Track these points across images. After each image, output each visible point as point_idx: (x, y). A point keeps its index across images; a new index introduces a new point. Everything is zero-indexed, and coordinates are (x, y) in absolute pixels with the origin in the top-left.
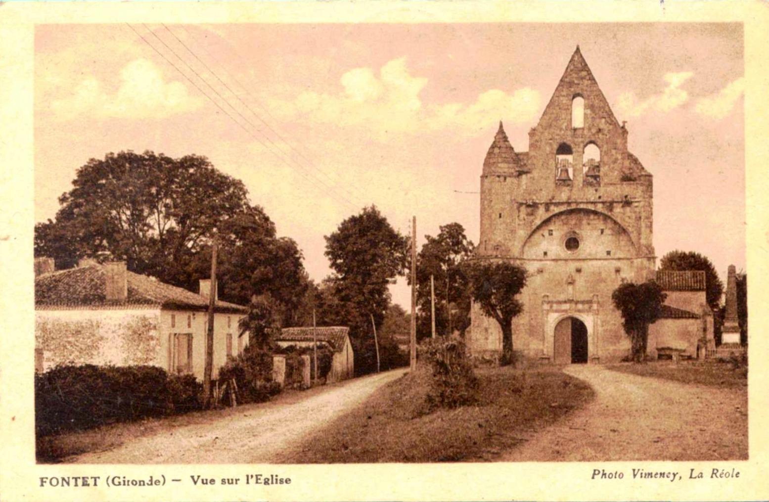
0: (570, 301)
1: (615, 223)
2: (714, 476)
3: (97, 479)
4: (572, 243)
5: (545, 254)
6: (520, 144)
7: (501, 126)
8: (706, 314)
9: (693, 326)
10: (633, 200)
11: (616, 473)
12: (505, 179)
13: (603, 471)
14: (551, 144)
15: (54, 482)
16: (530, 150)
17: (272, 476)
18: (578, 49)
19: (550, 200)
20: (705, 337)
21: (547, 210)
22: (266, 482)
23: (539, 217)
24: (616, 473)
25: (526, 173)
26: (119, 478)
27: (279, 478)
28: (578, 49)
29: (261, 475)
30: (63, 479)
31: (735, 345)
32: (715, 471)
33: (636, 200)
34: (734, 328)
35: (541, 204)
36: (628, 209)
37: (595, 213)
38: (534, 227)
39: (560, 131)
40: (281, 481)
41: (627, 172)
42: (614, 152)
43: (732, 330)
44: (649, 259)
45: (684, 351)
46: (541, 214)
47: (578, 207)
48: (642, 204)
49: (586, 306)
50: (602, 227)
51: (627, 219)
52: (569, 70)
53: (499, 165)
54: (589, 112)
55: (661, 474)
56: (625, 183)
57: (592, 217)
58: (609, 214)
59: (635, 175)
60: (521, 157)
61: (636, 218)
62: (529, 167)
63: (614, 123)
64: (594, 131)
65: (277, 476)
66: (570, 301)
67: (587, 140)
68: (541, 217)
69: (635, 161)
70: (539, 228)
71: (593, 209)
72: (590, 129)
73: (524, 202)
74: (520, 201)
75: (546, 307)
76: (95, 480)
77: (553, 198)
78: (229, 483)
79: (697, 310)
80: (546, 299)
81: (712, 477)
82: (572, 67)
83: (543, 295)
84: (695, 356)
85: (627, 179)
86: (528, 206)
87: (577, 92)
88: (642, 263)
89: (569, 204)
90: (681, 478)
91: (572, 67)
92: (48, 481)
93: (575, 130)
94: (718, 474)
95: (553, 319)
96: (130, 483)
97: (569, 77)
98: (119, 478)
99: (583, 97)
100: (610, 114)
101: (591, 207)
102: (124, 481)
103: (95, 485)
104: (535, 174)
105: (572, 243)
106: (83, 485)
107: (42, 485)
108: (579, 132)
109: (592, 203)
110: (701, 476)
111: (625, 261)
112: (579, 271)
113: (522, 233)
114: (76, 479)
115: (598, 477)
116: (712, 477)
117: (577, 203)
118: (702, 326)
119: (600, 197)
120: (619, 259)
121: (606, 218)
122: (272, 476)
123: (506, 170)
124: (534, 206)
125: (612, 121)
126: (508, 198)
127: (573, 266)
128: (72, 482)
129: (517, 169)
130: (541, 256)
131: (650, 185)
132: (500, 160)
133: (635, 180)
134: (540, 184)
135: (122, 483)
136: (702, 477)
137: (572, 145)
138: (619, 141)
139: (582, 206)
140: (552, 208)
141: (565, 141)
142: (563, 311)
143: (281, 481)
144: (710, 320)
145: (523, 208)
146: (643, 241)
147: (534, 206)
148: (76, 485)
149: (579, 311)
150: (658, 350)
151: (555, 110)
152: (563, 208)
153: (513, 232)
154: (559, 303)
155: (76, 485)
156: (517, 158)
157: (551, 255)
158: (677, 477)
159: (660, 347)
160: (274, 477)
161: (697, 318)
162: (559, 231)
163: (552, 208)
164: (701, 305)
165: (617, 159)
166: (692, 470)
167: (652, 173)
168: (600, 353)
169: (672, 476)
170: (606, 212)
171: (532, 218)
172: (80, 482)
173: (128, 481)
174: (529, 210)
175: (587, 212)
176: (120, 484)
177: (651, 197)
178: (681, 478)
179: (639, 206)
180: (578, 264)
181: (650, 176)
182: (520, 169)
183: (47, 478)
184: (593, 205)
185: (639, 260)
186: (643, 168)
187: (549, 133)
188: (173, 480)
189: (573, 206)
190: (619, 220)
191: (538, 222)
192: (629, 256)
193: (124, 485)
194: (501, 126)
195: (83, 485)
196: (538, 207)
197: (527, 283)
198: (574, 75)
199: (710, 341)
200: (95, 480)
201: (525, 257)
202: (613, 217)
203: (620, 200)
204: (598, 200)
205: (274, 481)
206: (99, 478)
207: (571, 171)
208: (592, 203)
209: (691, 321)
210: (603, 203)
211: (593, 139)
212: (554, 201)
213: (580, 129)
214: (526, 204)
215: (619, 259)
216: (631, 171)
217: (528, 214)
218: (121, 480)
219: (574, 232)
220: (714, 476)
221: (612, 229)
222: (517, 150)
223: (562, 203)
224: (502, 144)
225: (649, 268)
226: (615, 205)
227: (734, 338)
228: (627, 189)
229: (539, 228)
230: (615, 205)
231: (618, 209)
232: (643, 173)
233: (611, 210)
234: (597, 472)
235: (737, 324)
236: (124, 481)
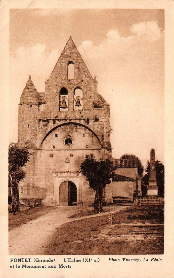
0: (67, 172)
1: (90, 130)
2: (152, 260)
3: (30, 259)
4: (68, 141)
5: (54, 147)
6: (41, 88)
7: (30, 78)
8: (137, 179)
9: (132, 185)
10: (99, 118)
11: (117, 259)
12: (31, 106)
13: (113, 258)
14: (57, 88)
15: (16, 260)
16: (45, 91)
17: (75, 259)
18: (71, 37)
19: (56, 118)
20: (137, 190)
21: (54, 123)
22: (72, 261)
23: (49, 127)
24: (117, 259)
25: (44, 103)
26: (38, 259)
27: (77, 260)
28: (71, 37)
29: (71, 259)
30: (19, 259)
31: (155, 197)
32: (153, 259)
33: (101, 118)
34: (154, 186)
35: (51, 120)
36: (97, 123)
37: (80, 125)
38: (47, 133)
39: (62, 80)
40: (78, 261)
41: (96, 103)
42: (90, 92)
43: (152, 188)
44: (108, 150)
45: (127, 198)
46: (51, 125)
47: (71, 122)
48: (104, 120)
49: (76, 174)
50: (83, 133)
51: (96, 128)
52: (66, 49)
53: (28, 98)
54: (77, 70)
55: (133, 260)
56: (95, 109)
57: (78, 127)
58: (87, 126)
59: (101, 105)
60: (41, 95)
61: (101, 127)
62: (45, 100)
63: (90, 77)
64: (79, 81)
65: (76, 259)
66: (67, 172)
67: (76, 86)
68: (51, 128)
69: (101, 98)
70: (51, 132)
71: (79, 123)
72: (77, 80)
73: (42, 119)
74: (40, 118)
75: (55, 175)
76: (23, 260)
77: (57, 117)
78: (47, 260)
79: (133, 177)
80: (54, 171)
81: (151, 261)
82: (67, 47)
83: (53, 168)
84: (132, 200)
85: (96, 106)
86: (44, 121)
87: (70, 60)
88: (105, 151)
89: (66, 120)
90: (140, 261)
91: (67, 47)
92: (13, 260)
93: (69, 80)
94: (154, 260)
95: (58, 182)
96: (42, 261)
97: (66, 52)
98: (38, 259)
99: (73, 64)
100: (88, 73)
101: (77, 122)
102: (40, 260)
103: (30, 261)
104: (48, 104)
105: (68, 141)
106: (25, 261)
107: (11, 262)
108: (71, 82)
109: (78, 119)
110: (147, 260)
111: (95, 151)
112: (72, 156)
113: (41, 136)
114: (23, 259)
115: (111, 261)
116: (151, 261)
117: (71, 120)
118: (136, 184)
119: (82, 117)
120: (93, 150)
121: (86, 127)
122: (75, 259)
123: (32, 101)
124: (48, 121)
125: (89, 76)
126: (33, 116)
127: (69, 153)
128: (22, 260)
129: (38, 101)
130: (52, 148)
131: (109, 110)
132: (28, 95)
133: (101, 107)
134: (50, 108)
135: (39, 261)
136: (148, 261)
137: (68, 89)
138: (92, 86)
139: (72, 121)
140: (57, 122)
141: (64, 86)
142: (64, 177)
143: (78, 261)
144: (140, 182)
145: (41, 122)
146: (105, 140)
147: (48, 121)
148: (23, 261)
149: (72, 177)
150: (113, 198)
151: (59, 70)
152: (63, 122)
153: (35, 135)
154: (62, 173)
155: (23, 261)
156: (38, 96)
157: (56, 147)
158: (139, 260)
159: (114, 196)
160: (75, 259)
161: (133, 181)
162: (61, 134)
163: (57, 122)
164: (135, 175)
165: (91, 97)
166: (144, 258)
167: (110, 104)
168: (83, 200)
169: (137, 260)
170: (85, 124)
171: (45, 127)
172: (24, 260)
173: (41, 260)
174: (45, 123)
175: (76, 124)
176: (38, 261)
177: (109, 117)
178: (140, 261)
179: (102, 120)
180: (72, 152)
181: (108, 105)
182: (40, 101)
183: (13, 259)
184: (79, 121)
185: (103, 150)
186: (105, 102)
187: (56, 82)
188: (98, 258)
189: (68, 121)
190: (92, 129)
191: (49, 130)
192: (98, 148)
193: (40, 261)
194: (30, 78)
195: (25, 261)
196: (49, 122)
197: (29, 159)
198: (68, 51)
199: (139, 192)
200: (23, 260)
201: (43, 149)
202: (89, 127)
203: (93, 118)
204: (81, 118)
205: (75, 261)
206: (31, 259)
207: (67, 103)
208: (78, 119)
209: (131, 182)
210: (84, 120)
211: (79, 85)
212: (58, 118)
213: (72, 80)
214: (42, 120)
215: (93, 150)
216: (99, 103)
217: (44, 126)
218: (39, 260)
219: (69, 136)
220: (152, 260)
221: (89, 133)
222: (38, 91)
223: (63, 120)
224: (30, 87)
225: (108, 154)
226: (90, 120)
227: (155, 192)
228: (96, 112)
229: (51, 132)
230: (90, 120)
231: (91, 123)
232: (105, 104)
233: (88, 123)
234: (110, 259)
235: (156, 184)
236: (40, 260)
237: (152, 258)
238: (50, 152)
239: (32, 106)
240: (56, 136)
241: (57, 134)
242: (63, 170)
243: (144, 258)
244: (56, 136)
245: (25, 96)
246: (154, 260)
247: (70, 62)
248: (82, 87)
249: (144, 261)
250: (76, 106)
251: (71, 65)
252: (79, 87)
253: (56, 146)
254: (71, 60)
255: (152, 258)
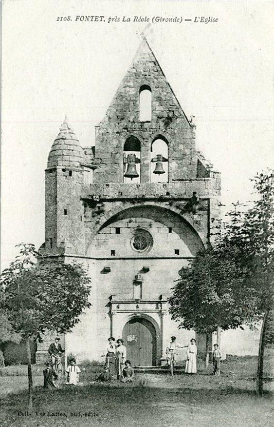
5: (113, 252)
12: (70, 174)
32: (136, 18)
67: (155, 135)
99: (151, 91)
108: (146, 125)
166: (124, 17)
237: (135, 17)
238: (105, 264)
239: (73, 173)
240: (118, 231)
241: (119, 227)
242: (129, 297)
243: (124, 17)
244: (118, 231)
245: (58, 154)
246: (138, 20)
247: (144, 87)
248: (152, 86)
249: (123, 21)
250: (178, 254)
251: (146, 92)
252: (160, 137)
253: (116, 252)
254: (146, 83)
255: (135, 17)
